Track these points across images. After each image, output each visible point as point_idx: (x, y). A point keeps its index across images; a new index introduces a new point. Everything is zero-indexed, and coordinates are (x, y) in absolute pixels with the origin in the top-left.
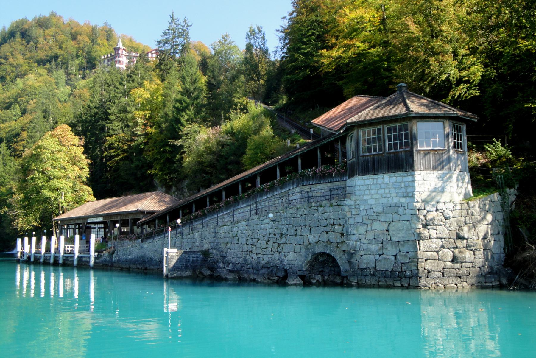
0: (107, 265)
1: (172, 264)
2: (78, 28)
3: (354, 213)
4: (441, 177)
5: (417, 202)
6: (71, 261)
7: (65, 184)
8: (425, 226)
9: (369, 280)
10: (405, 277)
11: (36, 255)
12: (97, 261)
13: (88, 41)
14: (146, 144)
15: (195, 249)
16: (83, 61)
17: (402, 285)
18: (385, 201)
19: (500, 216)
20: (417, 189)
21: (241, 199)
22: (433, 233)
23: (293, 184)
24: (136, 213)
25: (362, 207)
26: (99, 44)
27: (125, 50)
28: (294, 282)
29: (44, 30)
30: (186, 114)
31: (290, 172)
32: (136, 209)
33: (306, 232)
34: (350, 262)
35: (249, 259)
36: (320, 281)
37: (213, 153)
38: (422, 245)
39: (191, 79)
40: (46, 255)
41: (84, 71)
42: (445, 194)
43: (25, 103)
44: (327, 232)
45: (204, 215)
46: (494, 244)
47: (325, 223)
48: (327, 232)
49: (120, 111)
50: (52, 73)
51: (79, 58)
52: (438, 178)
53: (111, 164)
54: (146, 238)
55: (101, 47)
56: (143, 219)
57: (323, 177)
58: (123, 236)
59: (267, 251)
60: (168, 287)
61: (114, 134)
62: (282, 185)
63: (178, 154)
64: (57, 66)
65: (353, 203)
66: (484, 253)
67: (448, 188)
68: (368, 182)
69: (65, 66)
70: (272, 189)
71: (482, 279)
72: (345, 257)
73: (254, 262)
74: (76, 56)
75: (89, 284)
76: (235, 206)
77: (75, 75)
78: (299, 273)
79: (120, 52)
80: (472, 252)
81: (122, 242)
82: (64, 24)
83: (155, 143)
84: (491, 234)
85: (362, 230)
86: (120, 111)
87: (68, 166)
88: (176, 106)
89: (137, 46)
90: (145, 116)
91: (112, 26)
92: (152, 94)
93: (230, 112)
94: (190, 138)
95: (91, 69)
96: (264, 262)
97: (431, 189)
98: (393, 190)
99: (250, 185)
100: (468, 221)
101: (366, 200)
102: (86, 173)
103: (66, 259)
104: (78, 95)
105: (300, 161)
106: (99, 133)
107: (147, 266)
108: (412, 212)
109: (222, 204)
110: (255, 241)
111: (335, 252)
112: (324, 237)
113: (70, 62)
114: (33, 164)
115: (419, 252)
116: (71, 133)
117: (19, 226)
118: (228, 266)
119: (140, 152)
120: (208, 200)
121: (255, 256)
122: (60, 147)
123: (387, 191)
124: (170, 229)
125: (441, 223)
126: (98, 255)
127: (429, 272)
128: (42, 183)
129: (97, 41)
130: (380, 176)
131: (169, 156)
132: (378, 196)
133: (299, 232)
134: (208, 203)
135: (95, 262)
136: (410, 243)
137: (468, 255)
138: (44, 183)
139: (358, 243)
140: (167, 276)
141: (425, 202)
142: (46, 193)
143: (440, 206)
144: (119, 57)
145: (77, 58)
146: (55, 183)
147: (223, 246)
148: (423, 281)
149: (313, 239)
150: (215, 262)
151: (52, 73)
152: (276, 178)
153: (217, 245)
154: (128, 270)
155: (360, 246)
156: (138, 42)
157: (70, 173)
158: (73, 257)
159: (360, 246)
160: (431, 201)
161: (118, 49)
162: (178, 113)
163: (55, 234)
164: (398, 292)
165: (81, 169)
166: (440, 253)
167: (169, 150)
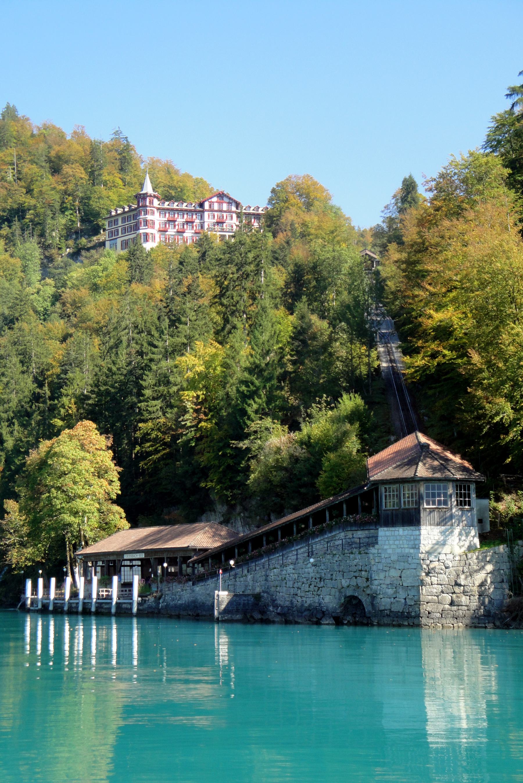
0: (153, 613)
1: (223, 607)
2: (62, 148)
3: (377, 561)
4: (443, 533)
5: (422, 553)
6: (106, 608)
8: (427, 574)
9: (386, 620)
10: (411, 617)
11: (56, 601)
12: (141, 608)
13: (83, 176)
14: (198, 440)
15: (248, 592)
16: (74, 219)
17: (409, 625)
18: (399, 551)
19: (506, 567)
20: (422, 542)
21: (295, 540)
22: (434, 580)
23: (339, 529)
24: (186, 549)
25: (383, 555)
26: (105, 184)
27: (157, 198)
28: (327, 622)
30: (255, 402)
31: (337, 517)
32: (185, 545)
33: (339, 577)
34: (373, 605)
35: (295, 602)
36: (351, 621)
37: (285, 469)
38: (424, 590)
39: (262, 350)
40: (71, 601)
41: (76, 239)
42: (446, 546)
44: (356, 577)
45: (260, 556)
46: (493, 591)
47: (355, 569)
48: (356, 577)
49: (159, 382)
50: (14, 245)
51: (66, 213)
52: (441, 533)
53: (146, 464)
54: (198, 581)
55: (110, 188)
56: (195, 558)
57: (362, 525)
58: (171, 578)
59: (310, 594)
60: (219, 628)
61: (150, 419)
62: (331, 529)
63: (243, 459)
64: (23, 230)
65: (376, 551)
66: (479, 598)
67: (449, 542)
68: (388, 533)
69: (37, 232)
70: (322, 532)
71: (476, 621)
72: (369, 600)
73: (299, 604)
74: (60, 210)
75: (131, 636)
76: (290, 548)
77: (60, 249)
78: (333, 614)
79: (148, 204)
80: (468, 597)
81: (170, 585)
82: (33, 136)
83: (211, 442)
84: (491, 582)
85: (382, 575)
86: (158, 383)
87: (95, 481)
88: (241, 389)
89: (181, 184)
90: (198, 397)
91: (129, 140)
92: (208, 365)
93: (313, 408)
94: (260, 438)
95: (90, 236)
96: (306, 605)
97: (434, 542)
98: (405, 541)
99: (303, 526)
100: (466, 570)
101: (386, 549)
102: (116, 489)
103: (99, 605)
104: (69, 300)
105: (344, 506)
106: (126, 415)
107: (199, 611)
108: (417, 561)
109: (277, 544)
110: (300, 584)
111: (362, 595)
112: (354, 582)
113: (49, 221)
114: (49, 479)
115: (421, 596)
116: (97, 432)
117: (14, 561)
118: (277, 610)
119: (190, 451)
120: (264, 539)
121: (299, 599)
122: (82, 454)
123: (401, 542)
124: (221, 571)
125: (442, 572)
126: (142, 600)
127: (429, 613)
128: (61, 504)
129: (100, 175)
130: (397, 529)
131: (231, 462)
132: (395, 547)
133: (334, 577)
134: (264, 543)
135: (138, 609)
136: (415, 588)
137: (464, 599)
138: (63, 505)
139: (379, 587)
140: (218, 618)
141: (429, 553)
142: (68, 518)
143: (442, 557)
144: (146, 213)
145: (63, 212)
146: (79, 504)
147: (273, 589)
148: (424, 621)
149: (345, 583)
150: (266, 606)
151: (14, 245)
152: (325, 522)
153: (268, 588)
154: (178, 617)
155: (380, 590)
156: (182, 172)
157: (96, 489)
158: (111, 603)
159: (380, 590)
160: (434, 552)
161: (144, 197)
162: (244, 401)
163: (70, 574)
164: (406, 630)
165: (111, 482)
166: (440, 597)
167: (231, 452)
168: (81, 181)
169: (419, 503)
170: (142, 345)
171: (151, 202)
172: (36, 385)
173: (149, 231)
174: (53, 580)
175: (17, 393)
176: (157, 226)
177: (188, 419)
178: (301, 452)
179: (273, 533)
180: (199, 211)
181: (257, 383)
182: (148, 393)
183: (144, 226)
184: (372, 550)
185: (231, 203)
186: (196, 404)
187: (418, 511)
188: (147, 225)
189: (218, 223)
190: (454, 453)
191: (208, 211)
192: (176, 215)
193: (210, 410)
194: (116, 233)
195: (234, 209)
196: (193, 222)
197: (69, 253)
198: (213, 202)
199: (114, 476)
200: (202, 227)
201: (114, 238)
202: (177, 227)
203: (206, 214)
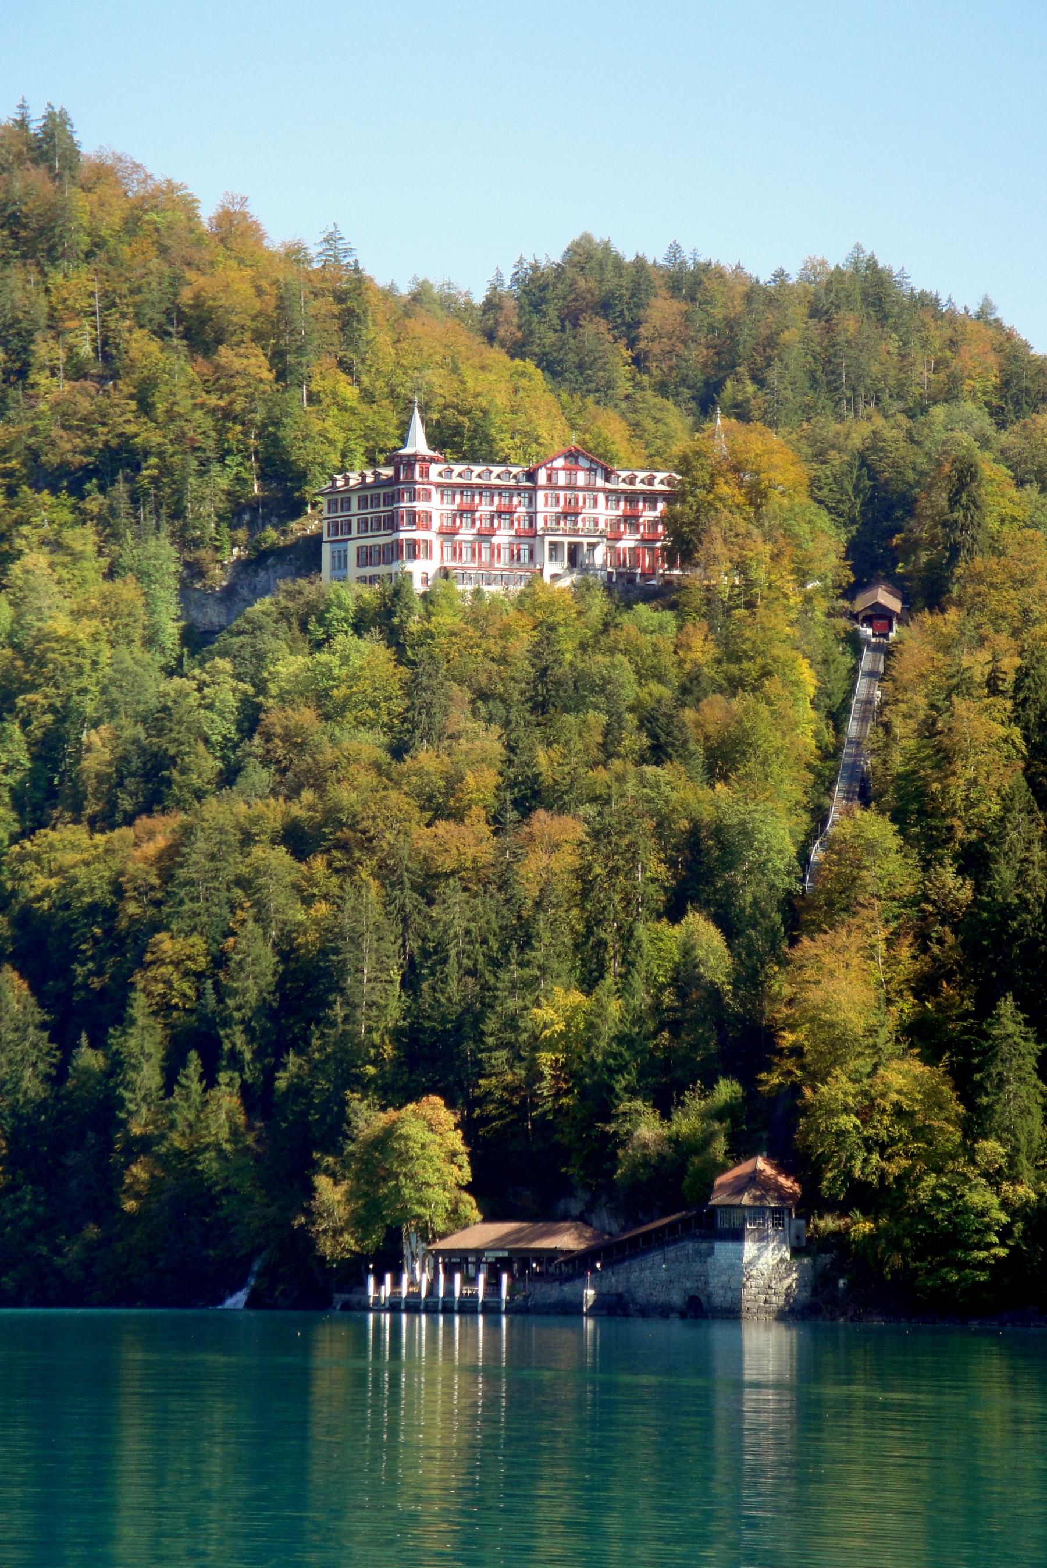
1: (590, 1304)
7: (437, 1194)
16: (245, 475)
29: (44, 274)
38: (745, 1292)
43: (44, 713)
45: (623, 1260)
62: (682, 1239)
64: (135, 500)
70: (675, 1241)
77: (217, 549)
90: (557, 1060)
102: (466, 1175)
103: (461, 1304)
122: (431, 1136)
137: (774, 1299)
144: (413, 498)
146: (428, 1193)
148: (744, 1314)
149: (688, 1285)
162: (611, 1077)
165: (460, 1167)
168: (262, 387)
169: (743, 1224)
170: (476, 960)
171: (425, 473)
172: (277, 959)
173: (419, 535)
174: (388, 1277)
175: (255, 978)
176: (436, 524)
177: (545, 1087)
178: (667, 1150)
179: (634, 1240)
180: (526, 488)
181: (626, 1054)
182: (491, 1041)
183: (409, 524)
184: (710, 1260)
185: (595, 470)
186: (554, 1069)
187: (742, 1230)
188: (414, 523)
189: (565, 515)
190: (787, 1177)
191: (544, 488)
192: (477, 498)
193: (571, 1076)
194: (345, 529)
195: (600, 482)
196: (511, 513)
197: (239, 558)
198: (557, 469)
199: (464, 1160)
200: (532, 522)
201: (340, 537)
202: (478, 524)
203: (541, 495)
